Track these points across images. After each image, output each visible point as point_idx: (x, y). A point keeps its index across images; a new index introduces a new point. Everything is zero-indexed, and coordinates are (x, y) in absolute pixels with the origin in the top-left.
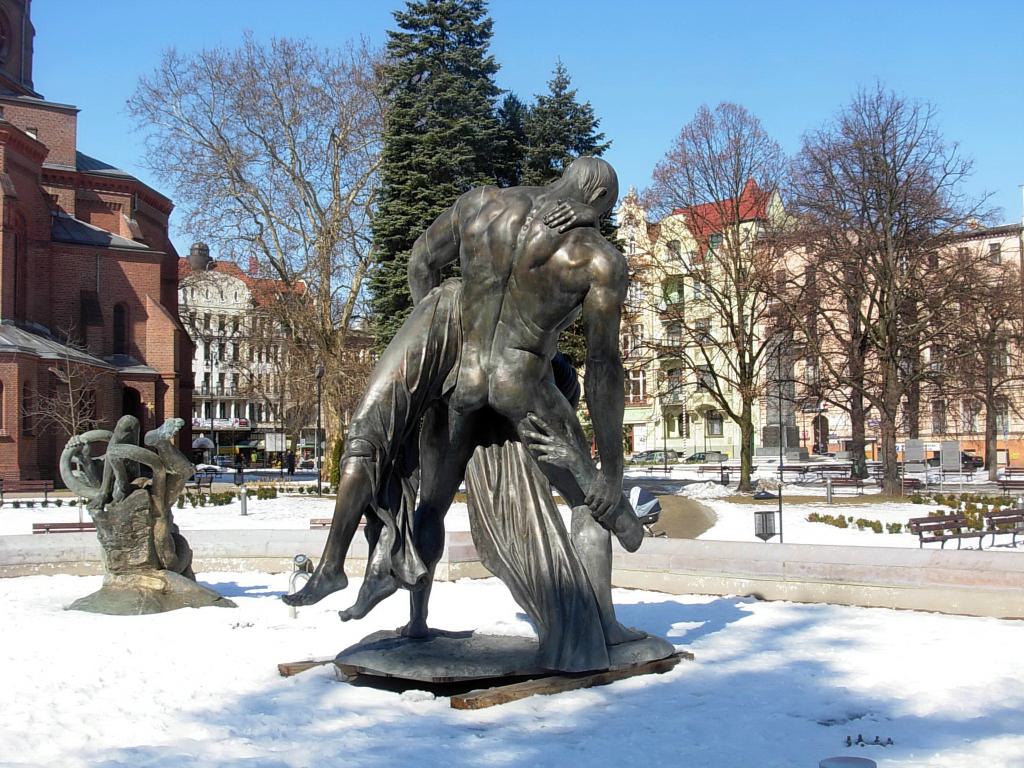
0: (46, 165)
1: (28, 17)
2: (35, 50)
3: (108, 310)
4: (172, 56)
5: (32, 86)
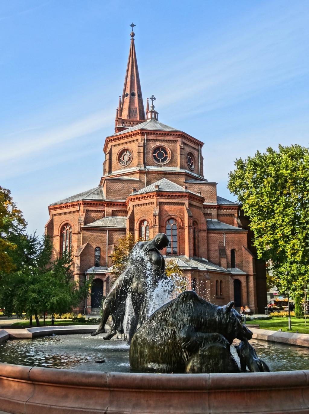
1: (201, 154)
2: (204, 164)
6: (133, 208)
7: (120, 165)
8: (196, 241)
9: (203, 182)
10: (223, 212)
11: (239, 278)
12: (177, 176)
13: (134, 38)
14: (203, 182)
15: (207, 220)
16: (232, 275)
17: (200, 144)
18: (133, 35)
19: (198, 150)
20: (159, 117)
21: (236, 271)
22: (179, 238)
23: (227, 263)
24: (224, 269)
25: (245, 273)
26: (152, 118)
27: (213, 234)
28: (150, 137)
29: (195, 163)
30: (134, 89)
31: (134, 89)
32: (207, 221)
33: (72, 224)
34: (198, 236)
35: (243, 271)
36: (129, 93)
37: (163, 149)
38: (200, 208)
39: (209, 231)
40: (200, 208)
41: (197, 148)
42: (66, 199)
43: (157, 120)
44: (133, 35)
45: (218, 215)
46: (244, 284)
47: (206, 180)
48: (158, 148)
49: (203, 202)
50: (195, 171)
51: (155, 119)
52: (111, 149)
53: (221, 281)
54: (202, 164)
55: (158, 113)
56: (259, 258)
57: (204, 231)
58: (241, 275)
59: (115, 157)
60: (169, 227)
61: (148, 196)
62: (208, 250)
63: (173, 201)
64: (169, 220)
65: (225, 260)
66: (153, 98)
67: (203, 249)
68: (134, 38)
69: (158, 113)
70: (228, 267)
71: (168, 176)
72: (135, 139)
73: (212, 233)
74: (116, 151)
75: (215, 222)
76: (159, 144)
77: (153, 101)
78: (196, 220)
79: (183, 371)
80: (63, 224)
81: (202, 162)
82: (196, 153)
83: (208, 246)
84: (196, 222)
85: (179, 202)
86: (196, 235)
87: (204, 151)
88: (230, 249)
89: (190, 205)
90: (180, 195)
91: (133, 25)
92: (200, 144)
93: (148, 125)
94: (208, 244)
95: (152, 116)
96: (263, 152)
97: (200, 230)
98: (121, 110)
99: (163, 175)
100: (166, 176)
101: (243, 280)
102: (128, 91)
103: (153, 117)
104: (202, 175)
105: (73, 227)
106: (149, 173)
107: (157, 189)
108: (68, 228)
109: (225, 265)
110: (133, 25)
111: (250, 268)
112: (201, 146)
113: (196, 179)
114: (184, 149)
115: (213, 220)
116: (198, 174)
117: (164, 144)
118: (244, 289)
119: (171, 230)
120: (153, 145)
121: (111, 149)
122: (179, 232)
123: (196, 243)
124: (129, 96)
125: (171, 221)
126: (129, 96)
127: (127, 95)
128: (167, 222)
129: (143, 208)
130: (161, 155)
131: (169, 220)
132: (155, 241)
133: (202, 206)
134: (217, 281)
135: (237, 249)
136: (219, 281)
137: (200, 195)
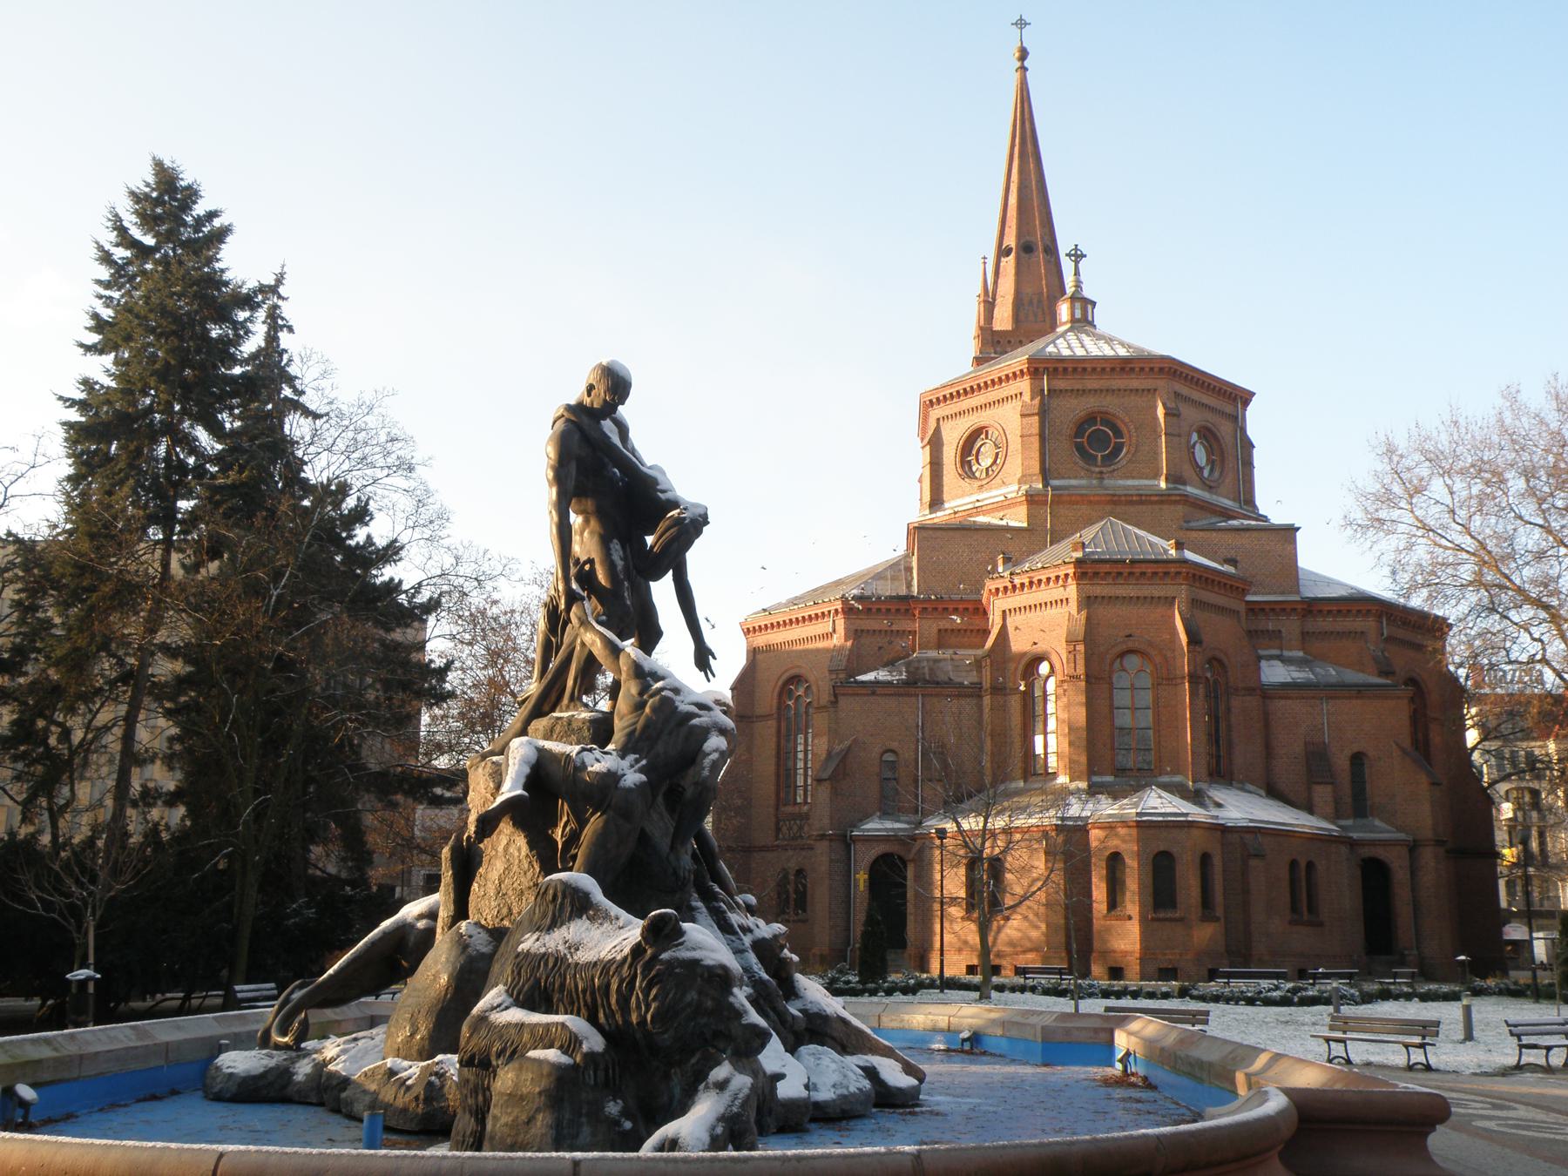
0: (1250, 598)
1: (1243, 430)
2: (1256, 464)
3: (1342, 762)
4: (1391, 451)
5: (1255, 507)
6: (1004, 619)
7: (966, 484)
8: (1222, 726)
10: (1325, 624)
11: (1381, 853)
12: (1156, 507)
16: (1353, 844)
17: (1243, 397)
18: (1023, 54)
20: (1100, 317)
21: (1378, 830)
22: (1157, 715)
23: (1337, 801)
25: (1402, 836)
26: (1073, 320)
28: (1061, 384)
29: (1223, 461)
30: (1032, 241)
31: (1032, 241)
33: (812, 679)
35: (1399, 829)
36: (1013, 245)
40: (1235, 613)
41: (1229, 409)
42: (794, 602)
43: (1092, 324)
44: (1023, 54)
45: (1305, 635)
46: (1400, 874)
47: (1265, 519)
48: (1091, 419)
49: (1244, 592)
51: (1083, 322)
52: (937, 431)
53: (1310, 866)
54: (1248, 464)
55: (1094, 304)
56: (633, 778)
59: (950, 454)
60: (1121, 680)
61: (1048, 579)
64: (1122, 655)
65: (1329, 788)
68: (1018, 64)
69: (1094, 304)
71: (1132, 509)
72: (1013, 393)
73: (1281, 698)
74: (953, 436)
76: (1091, 403)
77: (1077, 263)
80: (785, 677)
81: (1250, 456)
82: (1225, 429)
84: (1219, 661)
85: (1156, 594)
86: (1222, 707)
87: (1256, 421)
88: (1348, 752)
89: (1195, 603)
90: (1160, 569)
93: (1067, 345)
95: (1073, 314)
97: (1236, 690)
98: (989, 304)
99: (1108, 508)
100: (1119, 509)
101: (1397, 862)
102: (1011, 240)
103: (1078, 315)
105: (814, 688)
106: (1059, 503)
107: (1079, 554)
108: (801, 692)
112: (1246, 403)
113: (1227, 514)
116: (1237, 499)
117: (1110, 404)
119: (1128, 692)
120: (1076, 408)
121: (937, 431)
122: (1156, 699)
123: (1222, 733)
124: (1013, 255)
125: (1133, 662)
126: (1013, 255)
127: (1008, 252)
128: (1117, 664)
129: (1034, 617)
130: (1099, 440)
131: (1122, 655)
132: (633, 731)
133: (1242, 608)
134: (1293, 864)
135: (1371, 753)
136: (1303, 864)
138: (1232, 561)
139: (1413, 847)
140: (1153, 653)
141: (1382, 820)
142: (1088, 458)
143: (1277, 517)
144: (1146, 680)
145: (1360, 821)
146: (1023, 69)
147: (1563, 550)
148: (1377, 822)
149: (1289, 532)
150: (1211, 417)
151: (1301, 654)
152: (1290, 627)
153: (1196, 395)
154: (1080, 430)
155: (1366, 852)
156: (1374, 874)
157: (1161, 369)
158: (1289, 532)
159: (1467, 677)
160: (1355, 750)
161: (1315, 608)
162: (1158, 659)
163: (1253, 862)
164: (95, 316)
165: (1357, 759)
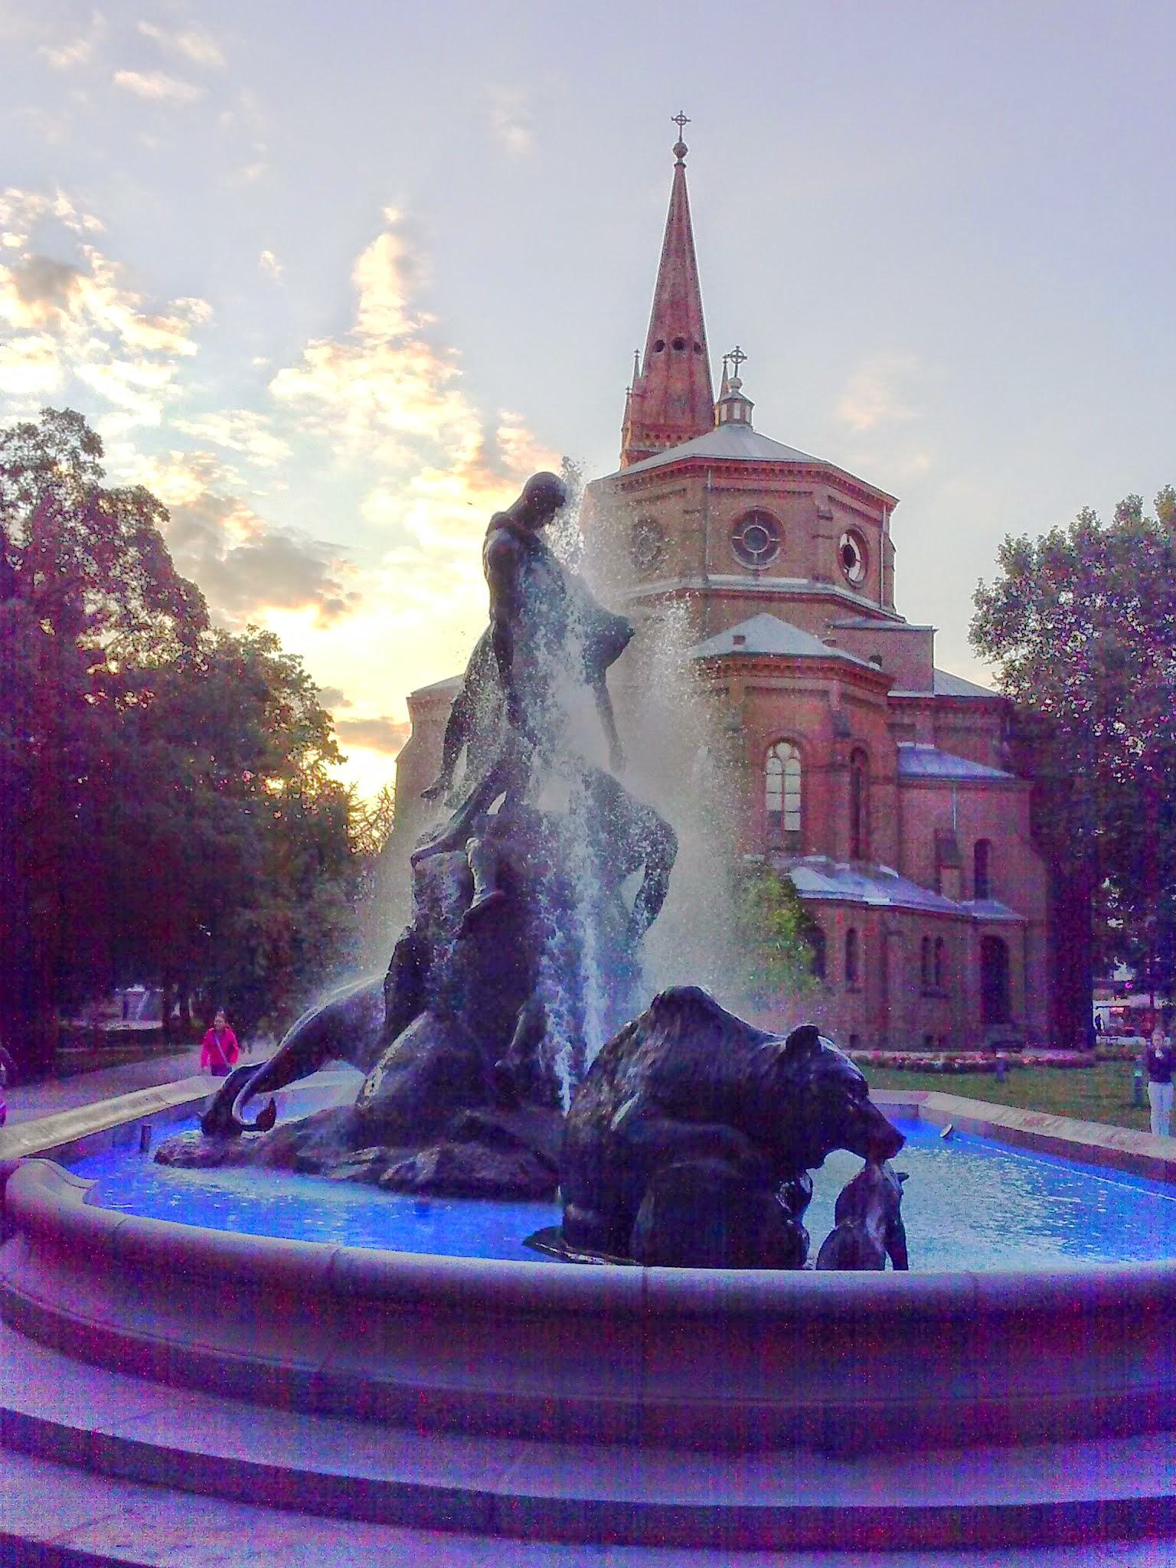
1: (887, 535)
8: (863, 813)
9: (893, 624)
11: (1002, 933)
13: (684, 160)
14: (893, 624)
15: (900, 745)
16: (975, 923)
17: (883, 503)
18: (681, 151)
19: (879, 523)
21: (992, 911)
23: (963, 887)
24: (947, 901)
27: (916, 791)
30: (677, 331)
31: (677, 331)
32: (899, 750)
34: (868, 796)
37: (766, 518)
38: (876, 707)
39: (903, 782)
40: (876, 707)
44: (681, 151)
45: (937, 729)
46: (1015, 953)
48: (751, 516)
50: (866, 590)
53: (939, 943)
57: (888, 780)
58: (1004, 924)
60: (773, 765)
62: (900, 842)
63: (164, 1437)
65: (956, 872)
66: (738, 356)
67: (882, 838)
68: (684, 160)
70: (963, 896)
71: (785, 606)
73: (915, 787)
75: (925, 752)
76: (748, 503)
78: (862, 745)
79: (792, 1255)
82: (870, 532)
83: (900, 832)
86: (863, 794)
87: (898, 527)
88: (973, 839)
91: (681, 120)
92: (883, 503)
93: (709, 445)
94: (901, 821)
96: (1106, 521)
104: (888, 602)
109: (956, 891)
110: (681, 120)
111: (1038, 898)
112: (890, 509)
113: (868, 614)
114: (830, 519)
115: (920, 746)
117: (771, 505)
118: (1015, 968)
130: (758, 538)
134: (926, 939)
137: (877, 667)
138: (877, 659)
139: (1025, 927)
140: (804, 742)
141: (1001, 901)
142: (747, 555)
143: (915, 621)
144: (795, 767)
145: (982, 902)
146: (680, 166)
147: (1173, 662)
148: (996, 904)
149: (925, 635)
150: (858, 521)
151: (931, 747)
152: (923, 721)
153: (847, 500)
154: (738, 524)
155: (990, 930)
156: (993, 952)
157: (818, 473)
158: (925, 635)
159: (80, 209)
160: (979, 837)
161: (944, 704)
162: (808, 748)
163: (894, 939)
164: (347, 704)
165: (982, 846)
